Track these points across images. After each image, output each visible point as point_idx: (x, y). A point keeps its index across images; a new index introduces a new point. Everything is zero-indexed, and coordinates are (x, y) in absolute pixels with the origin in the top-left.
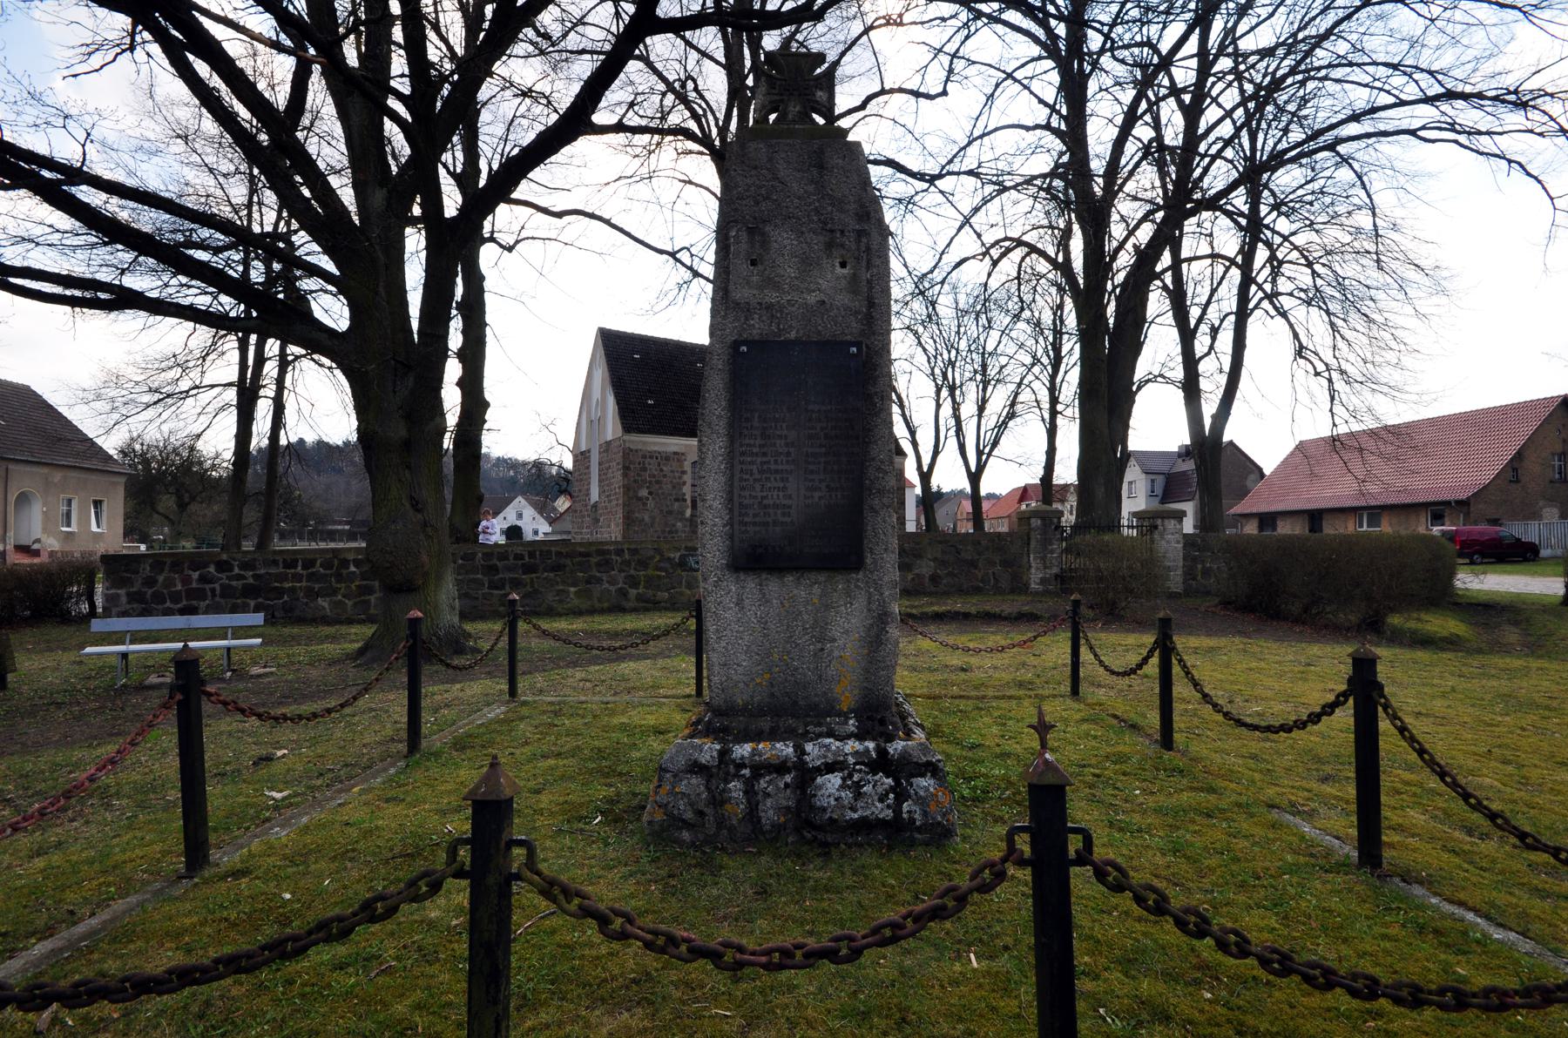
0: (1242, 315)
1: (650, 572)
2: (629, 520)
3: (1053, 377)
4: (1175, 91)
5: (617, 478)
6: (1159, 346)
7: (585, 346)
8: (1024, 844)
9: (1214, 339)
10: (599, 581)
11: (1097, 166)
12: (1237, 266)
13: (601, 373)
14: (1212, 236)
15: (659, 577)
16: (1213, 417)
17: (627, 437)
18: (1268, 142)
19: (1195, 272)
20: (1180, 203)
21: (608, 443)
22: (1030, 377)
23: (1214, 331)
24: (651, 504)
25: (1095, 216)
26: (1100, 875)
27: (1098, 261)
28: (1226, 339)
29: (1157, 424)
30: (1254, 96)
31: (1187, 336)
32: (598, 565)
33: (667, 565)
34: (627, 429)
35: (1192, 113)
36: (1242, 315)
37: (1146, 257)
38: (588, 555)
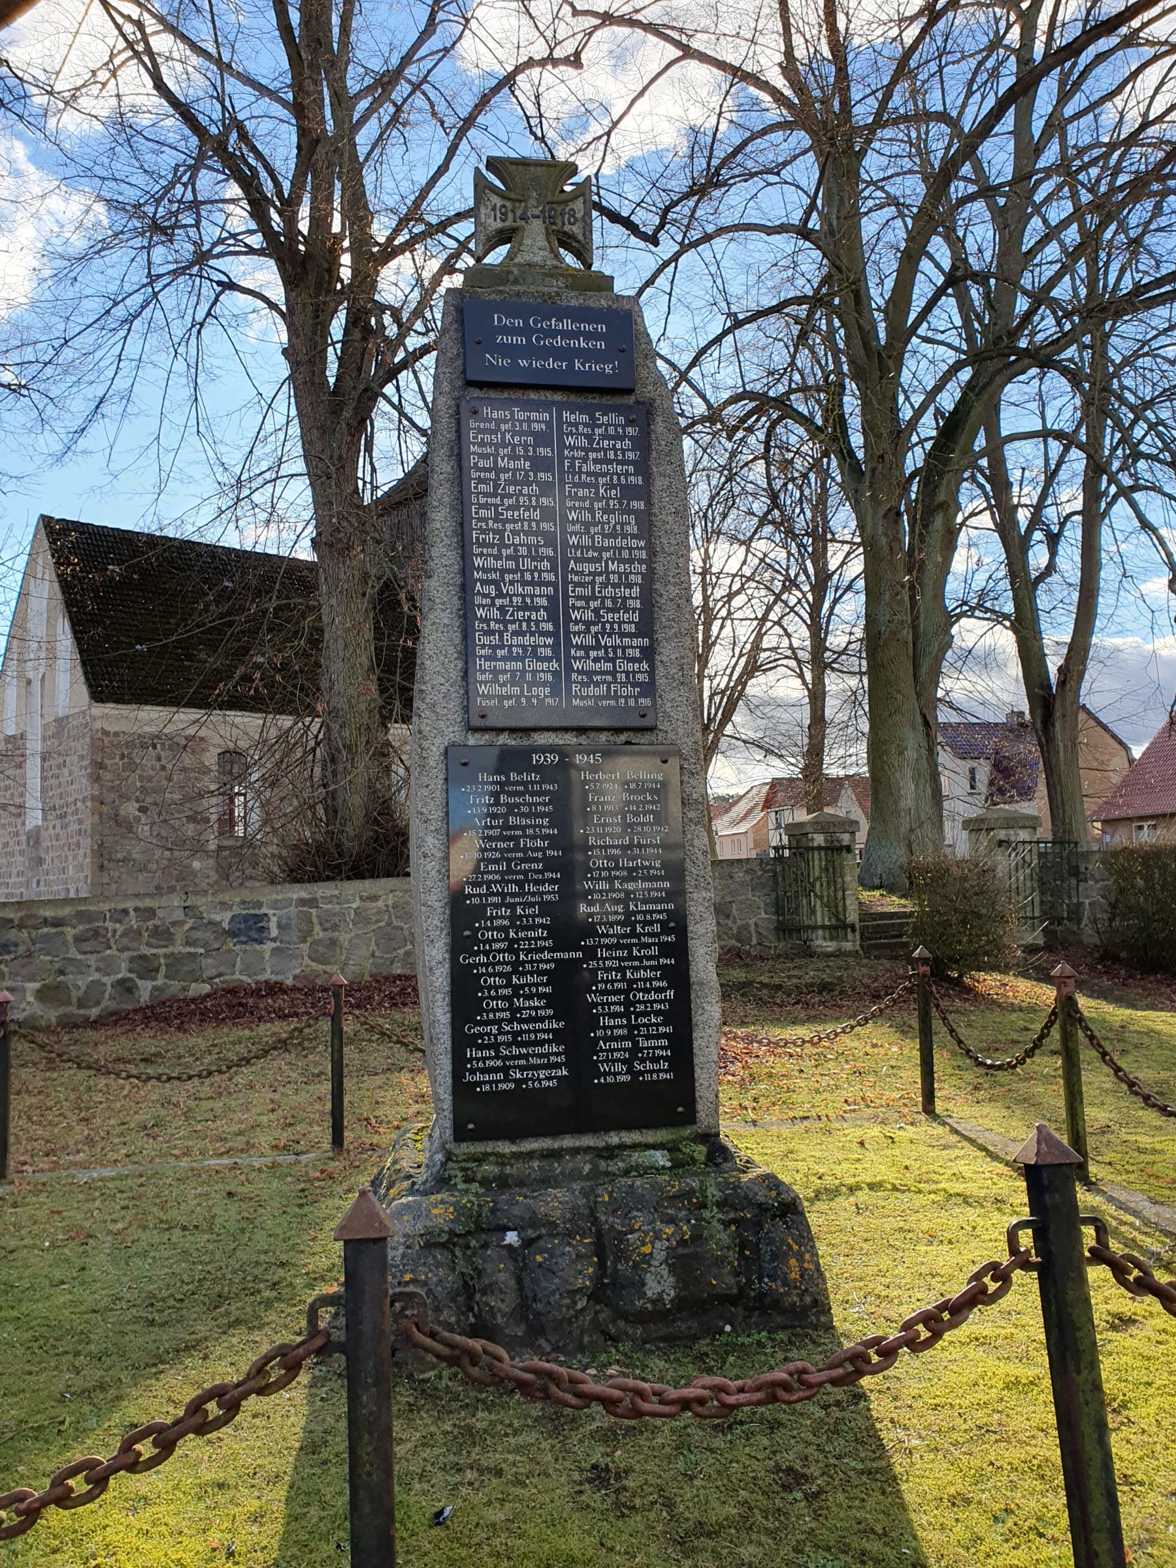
0: (1092, 518)
1: (179, 948)
2: (103, 858)
3: (815, 609)
4: (987, 191)
5: (80, 786)
6: (975, 559)
7: (21, 537)
8: (1026, 1239)
9: (1053, 553)
10: (82, 968)
11: (879, 294)
12: (1080, 447)
13: (47, 591)
14: (1034, 404)
15: (193, 955)
16: (1060, 670)
17: (99, 709)
18: (1120, 277)
19: (1024, 461)
20: (995, 356)
21: (61, 722)
22: (778, 609)
23: (1053, 540)
24: (144, 830)
25: (877, 366)
26: (1119, 1270)
27: (889, 433)
28: (1070, 559)
29: (982, 677)
30: (1095, 207)
31: (1015, 546)
32: (79, 939)
33: (209, 935)
34: (98, 695)
35: (1009, 224)
36: (1092, 518)
37: (953, 428)
38: (58, 923)
